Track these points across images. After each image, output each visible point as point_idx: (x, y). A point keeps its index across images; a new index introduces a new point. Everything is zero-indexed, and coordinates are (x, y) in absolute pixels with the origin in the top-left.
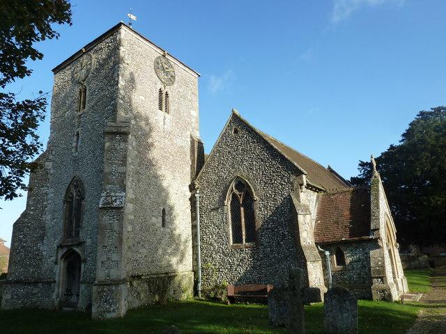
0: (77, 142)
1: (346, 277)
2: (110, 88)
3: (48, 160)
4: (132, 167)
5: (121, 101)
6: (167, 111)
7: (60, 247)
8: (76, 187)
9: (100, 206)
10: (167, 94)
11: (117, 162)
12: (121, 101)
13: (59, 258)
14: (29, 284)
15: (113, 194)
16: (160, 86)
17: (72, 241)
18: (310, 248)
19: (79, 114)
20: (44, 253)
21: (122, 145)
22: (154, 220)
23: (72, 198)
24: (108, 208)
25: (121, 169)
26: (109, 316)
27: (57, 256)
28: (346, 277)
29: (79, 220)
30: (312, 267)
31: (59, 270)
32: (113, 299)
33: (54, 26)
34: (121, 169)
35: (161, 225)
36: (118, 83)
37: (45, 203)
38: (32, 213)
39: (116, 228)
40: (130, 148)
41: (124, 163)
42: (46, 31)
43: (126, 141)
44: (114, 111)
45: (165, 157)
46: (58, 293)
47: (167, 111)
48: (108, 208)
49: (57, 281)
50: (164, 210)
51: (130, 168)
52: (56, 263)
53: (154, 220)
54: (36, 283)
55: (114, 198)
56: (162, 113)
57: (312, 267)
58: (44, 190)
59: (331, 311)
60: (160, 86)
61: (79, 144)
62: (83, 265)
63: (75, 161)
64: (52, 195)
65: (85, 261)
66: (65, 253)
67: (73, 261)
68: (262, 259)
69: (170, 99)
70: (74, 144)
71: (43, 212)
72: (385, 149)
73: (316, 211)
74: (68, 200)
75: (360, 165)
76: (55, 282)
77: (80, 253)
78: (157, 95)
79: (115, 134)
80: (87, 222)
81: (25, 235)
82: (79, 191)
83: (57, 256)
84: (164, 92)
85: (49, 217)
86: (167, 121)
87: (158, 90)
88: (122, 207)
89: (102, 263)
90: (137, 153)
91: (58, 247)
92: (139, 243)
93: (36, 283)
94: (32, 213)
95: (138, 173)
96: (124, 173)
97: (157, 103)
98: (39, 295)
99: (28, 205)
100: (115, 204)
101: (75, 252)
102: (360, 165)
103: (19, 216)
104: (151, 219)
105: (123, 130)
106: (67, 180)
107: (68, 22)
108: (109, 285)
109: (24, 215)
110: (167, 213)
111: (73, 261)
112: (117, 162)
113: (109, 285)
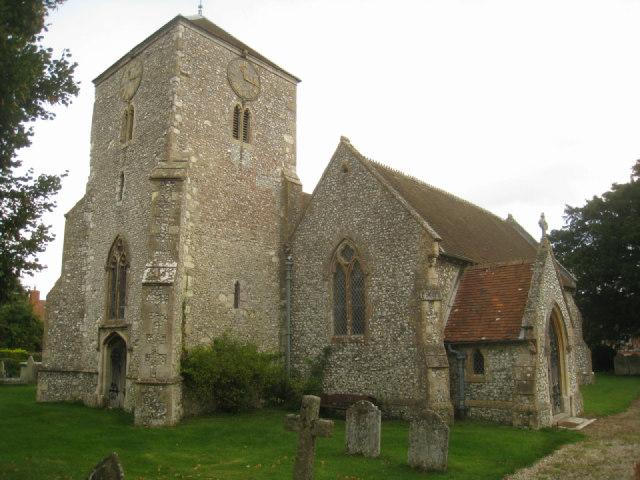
0: (122, 186)
1: (484, 391)
2: (162, 111)
3: (87, 209)
4: (191, 224)
5: (176, 131)
6: (246, 139)
7: (102, 329)
8: (120, 248)
9: (144, 281)
10: (247, 114)
11: (166, 219)
12: (176, 131)
13: (102, 341)
14: (68, 373)
15: (161, 265)
16: (235, 101)
17: (116, 322)
18: (435, 348)
19: (124, 146)
20: (85, 335)
21: (175, 196)
22: (222, 298)
23: (115, 264)
24: (153, 285)
25: (174, 229)
26: (155, 423)
27: (99, 340)
28: (484, 391)
29: (123, 295)
30: (434, 375)
31: (100, 360)
32: (159, 402)
33: (46, 105)
34: (174, 229)
35: (231, 305)
36: (172, 105)
37: (84, 269)
38: (68, 281)
39: (164, 312)
40: (188, 196)
41: (177, 222)
42: (35, 111)
43: (179, 190)
44: (167, 146)
45: (241, 207)
46: (102, 387)
47: (246, 139)
48: (153, 285)
49: (100, 373)
50: (237, 285)
51: (187, 224)
52: (98, 350)
53: (222, 298)
54: (75, 373)
55: (162, 271)
56: (237, 143)
57: (434, 375)
58: (83, 250)
59: (417, 441)
60: (235, 101)
61: (124, 189)
62: (128, 355)
63: (120, 212)
64: (92, 258)
65: (131, 350)
66: (109, 337)
67: (117, 348)
68: (371, 359)
69: (252, 120)
70: (118, 190)
71: (82, 282)
72: (608, 188)
73: (455, 293)
74: (111, 266)
75: (566, 211)
76: (97, 373)
77: (125, 339)
78: (230, 117)
79: (164, 180)
80: (134, 296)
81: (61, 310)
82: (123, 256)
83: (99, 340)
84: (243, 111)
85: (89, 288)
86: (247, 154)
87: (232, 109)
88: (171, 284)
89: (147, 355)
90: (198, 203)
91: (100, 329)
92: (200, 329)
93: (75, 373)
94: (68, 281)
95: (199, 232)
96: (177, 236)
97: (230, 128)
98: (80, 388)
99: (64, 271)
100: (163, 279)
101: (120, 338)
102: (566, 211)
103: (53, 285)
104: (217, 297)
105: (177, 173)
106: (109, 240)
107: (64, 102)
108: (157, 385)
109: (59, 283)
110: (241, 287)
111: (117, 348)
112: (166, 219)
113: (157, 385)
